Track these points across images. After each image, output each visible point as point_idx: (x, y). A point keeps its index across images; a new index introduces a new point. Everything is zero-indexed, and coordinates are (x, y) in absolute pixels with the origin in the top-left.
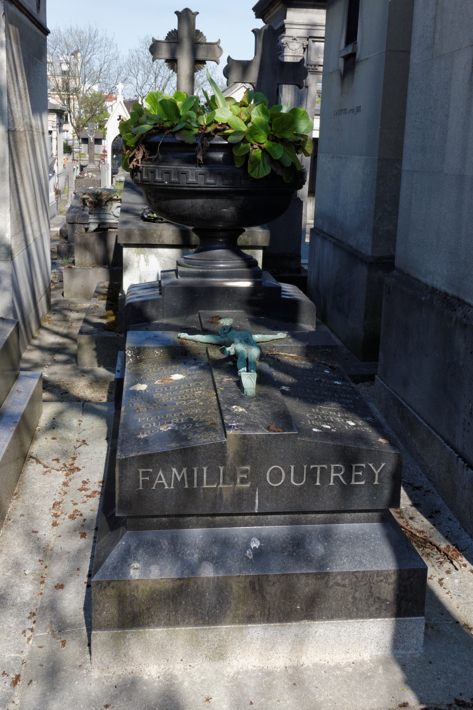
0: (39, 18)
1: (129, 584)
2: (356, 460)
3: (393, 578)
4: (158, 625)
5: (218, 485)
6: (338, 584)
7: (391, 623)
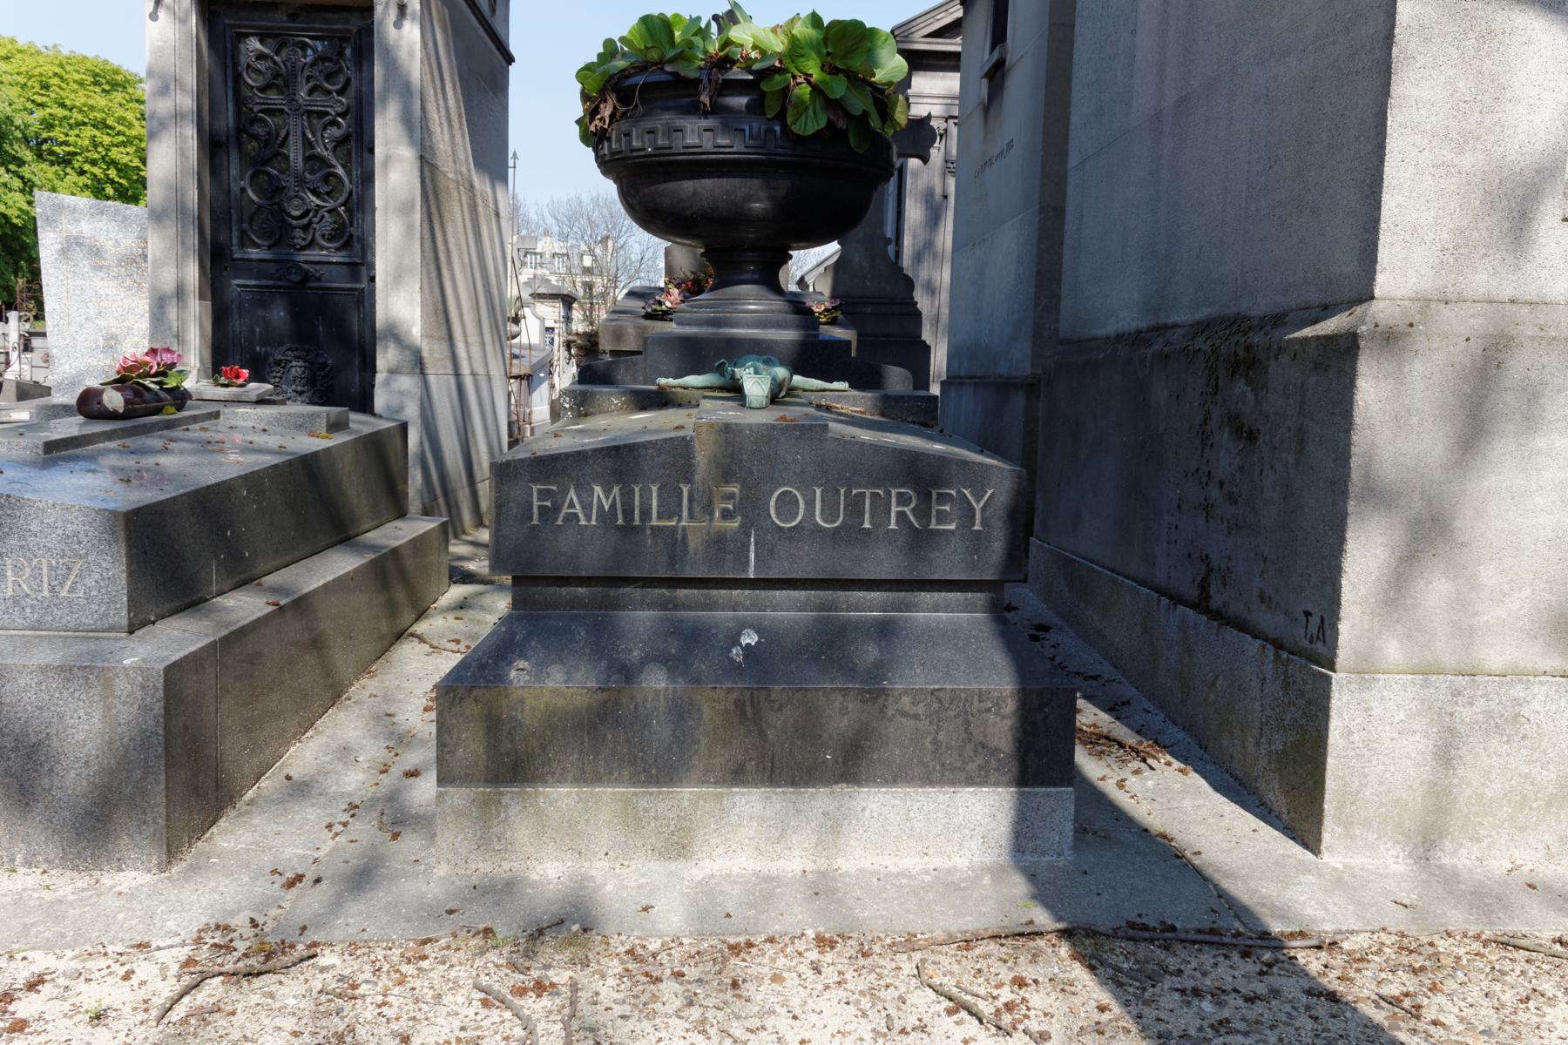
0: (497, 26)
1: (507, 696)
2: (938, 481)
3: (1010, 706)
4: (561, 781)
5: (679, 521)
6: (904, 714)
7: (1008, 797)
